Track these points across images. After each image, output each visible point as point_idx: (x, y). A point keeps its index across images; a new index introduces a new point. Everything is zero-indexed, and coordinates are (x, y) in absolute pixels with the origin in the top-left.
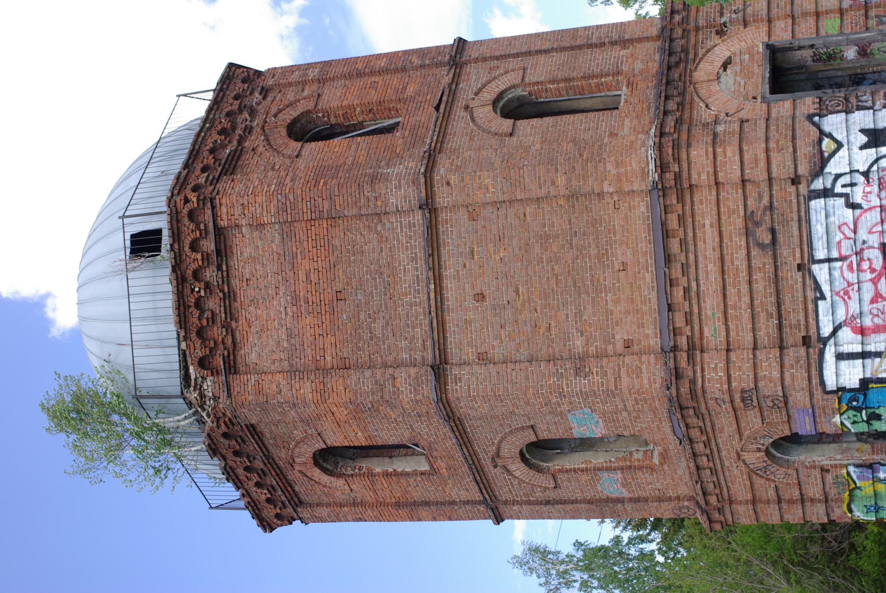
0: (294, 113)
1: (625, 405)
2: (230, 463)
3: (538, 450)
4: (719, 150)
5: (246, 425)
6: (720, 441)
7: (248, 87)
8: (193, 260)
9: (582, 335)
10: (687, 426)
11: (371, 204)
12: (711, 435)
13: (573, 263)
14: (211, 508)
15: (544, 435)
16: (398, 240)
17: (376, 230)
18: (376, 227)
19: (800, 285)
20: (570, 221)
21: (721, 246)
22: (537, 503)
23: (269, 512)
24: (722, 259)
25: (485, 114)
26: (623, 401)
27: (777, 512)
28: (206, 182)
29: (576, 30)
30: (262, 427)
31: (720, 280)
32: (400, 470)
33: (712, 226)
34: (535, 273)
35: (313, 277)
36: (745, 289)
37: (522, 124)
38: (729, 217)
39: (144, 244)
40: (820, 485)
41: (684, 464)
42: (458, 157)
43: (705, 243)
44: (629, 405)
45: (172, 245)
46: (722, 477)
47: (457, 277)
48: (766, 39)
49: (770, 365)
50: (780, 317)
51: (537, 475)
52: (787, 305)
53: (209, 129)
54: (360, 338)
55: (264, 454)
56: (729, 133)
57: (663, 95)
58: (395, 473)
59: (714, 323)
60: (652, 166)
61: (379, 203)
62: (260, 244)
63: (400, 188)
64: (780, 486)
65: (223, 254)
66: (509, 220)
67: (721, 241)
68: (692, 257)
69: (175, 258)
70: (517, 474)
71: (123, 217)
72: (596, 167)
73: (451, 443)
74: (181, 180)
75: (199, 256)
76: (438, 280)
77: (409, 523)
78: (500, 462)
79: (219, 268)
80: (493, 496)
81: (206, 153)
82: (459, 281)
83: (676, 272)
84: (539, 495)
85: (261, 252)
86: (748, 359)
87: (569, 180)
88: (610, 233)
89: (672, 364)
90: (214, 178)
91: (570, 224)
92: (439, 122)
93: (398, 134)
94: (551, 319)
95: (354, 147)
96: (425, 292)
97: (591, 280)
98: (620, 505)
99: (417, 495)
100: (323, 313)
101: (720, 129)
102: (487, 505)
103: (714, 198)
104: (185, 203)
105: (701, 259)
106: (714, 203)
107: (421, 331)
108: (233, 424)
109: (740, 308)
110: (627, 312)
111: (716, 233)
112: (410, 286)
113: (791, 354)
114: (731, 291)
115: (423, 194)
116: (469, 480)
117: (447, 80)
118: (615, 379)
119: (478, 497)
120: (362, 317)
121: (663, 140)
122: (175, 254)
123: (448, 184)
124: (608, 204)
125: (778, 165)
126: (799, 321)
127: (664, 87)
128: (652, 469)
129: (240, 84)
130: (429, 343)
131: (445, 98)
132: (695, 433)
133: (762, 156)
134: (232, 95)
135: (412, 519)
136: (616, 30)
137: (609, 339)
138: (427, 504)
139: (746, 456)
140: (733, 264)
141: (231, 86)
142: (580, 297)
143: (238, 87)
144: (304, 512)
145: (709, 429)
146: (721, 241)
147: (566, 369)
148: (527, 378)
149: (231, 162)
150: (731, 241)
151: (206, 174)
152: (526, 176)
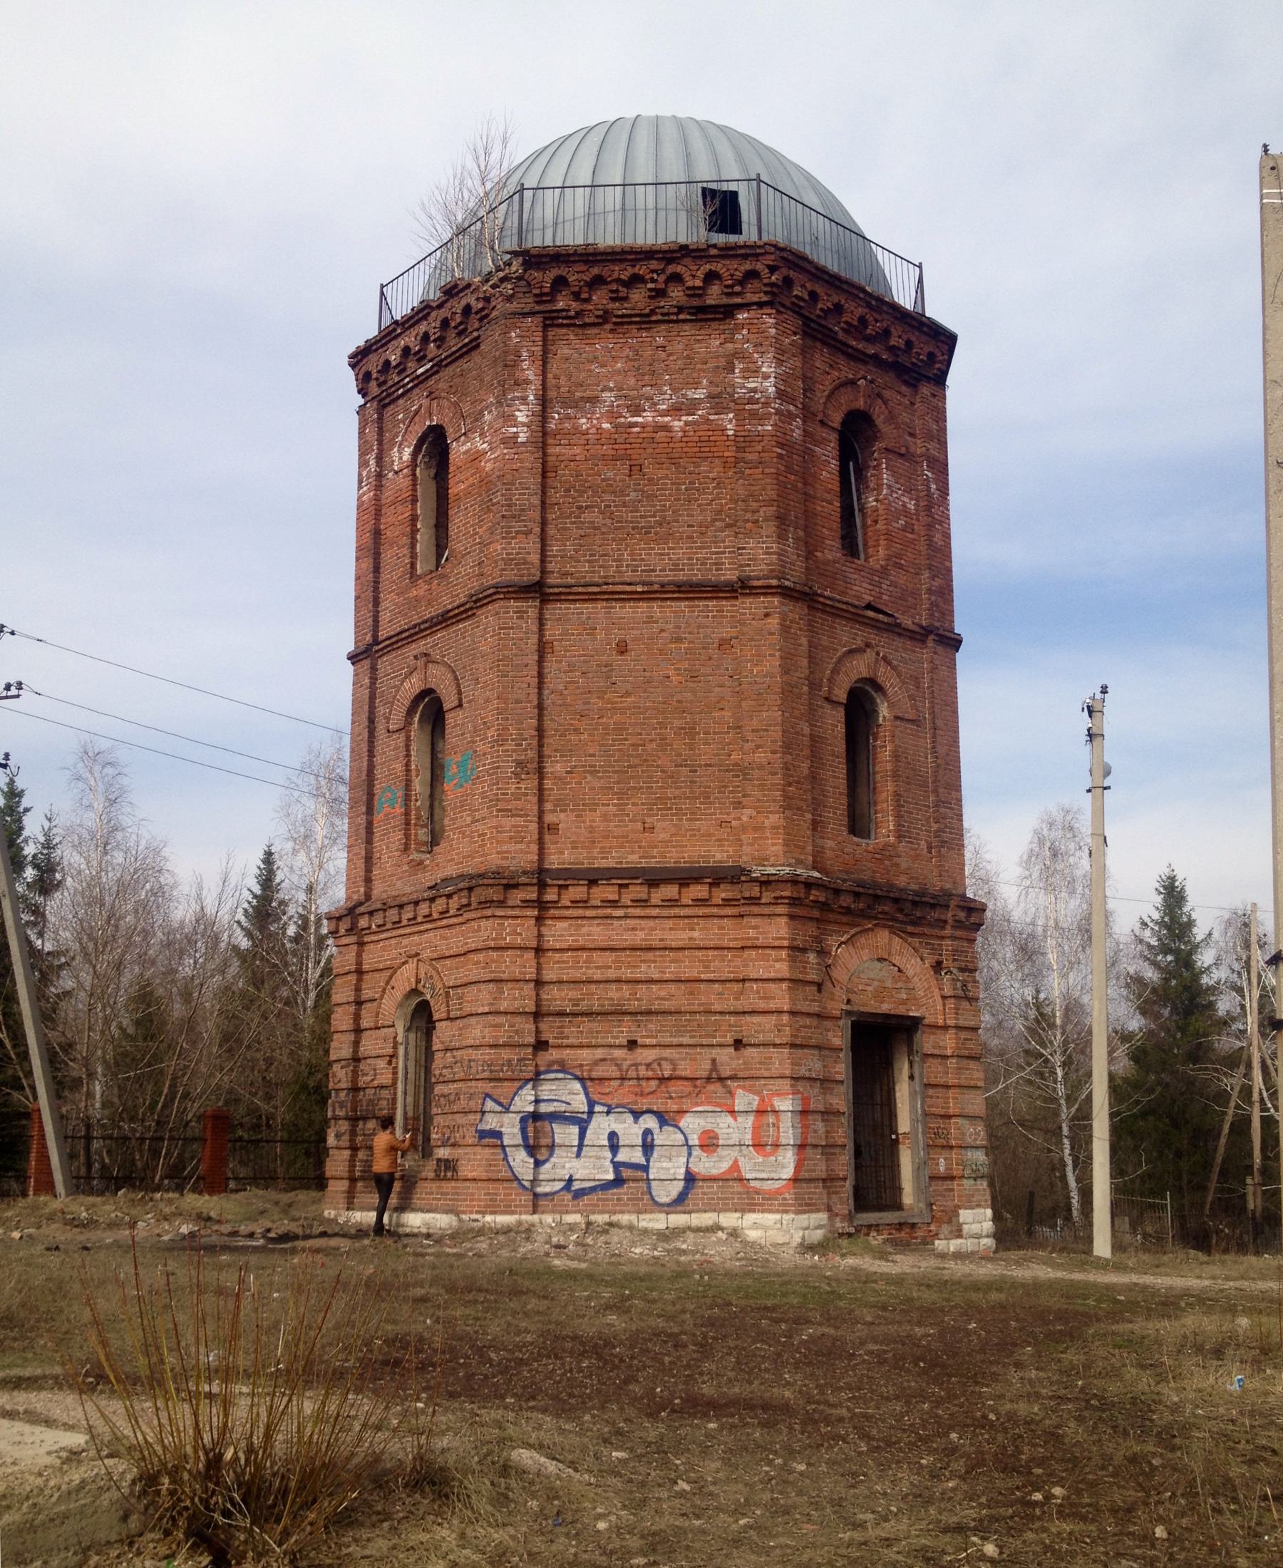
0: (879, 421)
1: (478, 821)
2: (434, 314)
3: (430, 708)
4: (784, 953)
5: (478, 337)
6: (431, 934)
7: (922, 361)
8: (694, 275)
9: (567, 772)
10: (449, 896)
11: (748, 516)
12: (439, 924)
13: (658, 766)
14: (382, 286)
15: (450, 719)
16: (701, 548)
17: (716, 520)
18: (720, 520)
19: (611, 1041)
20: (710, 765)
21: (665, 949)
22: (372, 708)
23: (373, 364)
24: (650, 949)
25: (860, 667)
26: (484, 818)
27: (344, 1000)
28: (796, 296)
29: (958, 788)
30: (475, 356)
31: (624, 945)
32: (418, 537)
33: (691, 939)
34: (648, 718)
35: (661, 435)
36: (611, 974)
37: (840, 714)
38: (700, 961)
39: (723, 208)
40: (373, 1053)
41: (408, 890)
42: (801, 630)
43: (671, 929)
44: (480, 827)
45: (715, 246)
46: (389, 934)
47: (650, 620)
48: (926, 1021)
49: (515, 999)
50: (575, 1015)
51: (404, 710)
52: (587, 1024)
53: (869, 305)
54: (581, 493)
55: (442, 361)
56: (805, 968)
57: (861, 890)
58: (414, 531)
59: (571, 935)
60: (771, 870)
61: (749, 525)
62: (709, 365)
63: (767, 553)
64: (375, 1004)
65: (700, 316)
66: (717, 689)
67: (671, 949)
68: (655, 912)
69: (698, 250)
70: (407, 685)
71: (759, 180)
72: (774, 801)
73: (447, 603)
74: (801, 263)
75: (698, 283)
76: (647, 596)
77: (354, 546)
78: (421, 663)
79: (681, 309)
80: (384, 652)
81: (835, 299)
82: (645, 623)
83: (638, 891)
84: (381, 710)
85: (699, 366)
86: (525, 973)
87: (761, 768)
88: (692, 813)
89: (523, 880)
90: (801, 307)
91: (706, 765)
92: (851, 609)
93: (839, 555)
94: (590, 735)
95: (828, 496)
96: (633, 579)
97: (634, 788)
98: (364, 809)
99: (388, 556)
100: (616, 447)
101: (812, 957)
102: (371, 645)
103: (725, 943)
104: (768, 266)
105: (651, 923)
106: (719, 943)
107: (583, 570)
108: (481, 320)
109: (587, 968)
110: (591, 830)
111: (681, 944)
112: (643, 560)
113: (527, 1026)
114: (609, 957)
115: (756, 583)
116: (403, 624)
117: (907, 621)
118: (510, 810)
119: (383, 634)
120: (607, 497)
121: (802, 886)
122: (703, 250)
123: (767, 615)
124: (728, 814)
125: (759, 1025)
126: (568, 1038)
127: (871, 892)
128: (406, 848)
129: (927, 349)
130: (569, 580)
131: (881, 617)
132: (440, 904)
133: (772, 1006)
134: (913, 339)
135: (359, 549)
136: (953, 839)
137: (561, 805)
138: (377, 569)
139: (412, 965)
140: (644, 961)
141: (924, 338)
142: (615, 772)
143: (923, 348)
144: (371, 408)
145: (445, 922)
146: (671, 949)
147: (526, 750)
148: (517, 702)
149: (821, 333)
150: (671, 962)
151: (807, 298)
152: (769, 713)
